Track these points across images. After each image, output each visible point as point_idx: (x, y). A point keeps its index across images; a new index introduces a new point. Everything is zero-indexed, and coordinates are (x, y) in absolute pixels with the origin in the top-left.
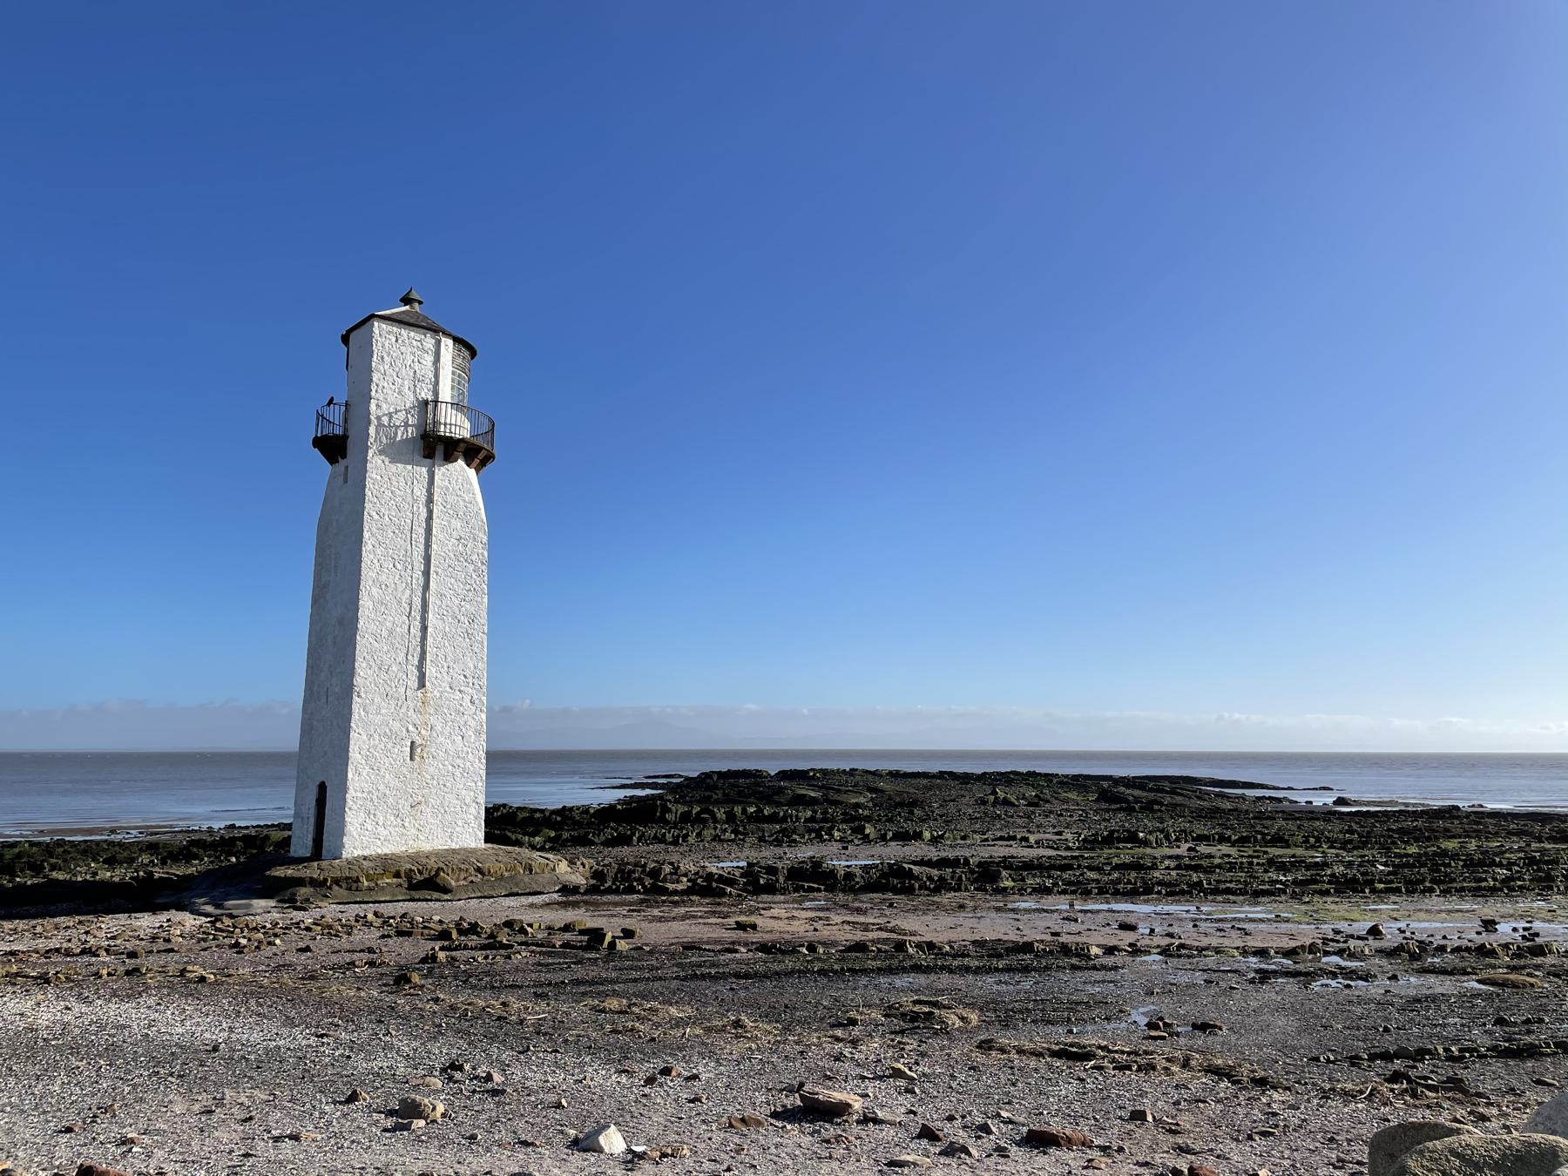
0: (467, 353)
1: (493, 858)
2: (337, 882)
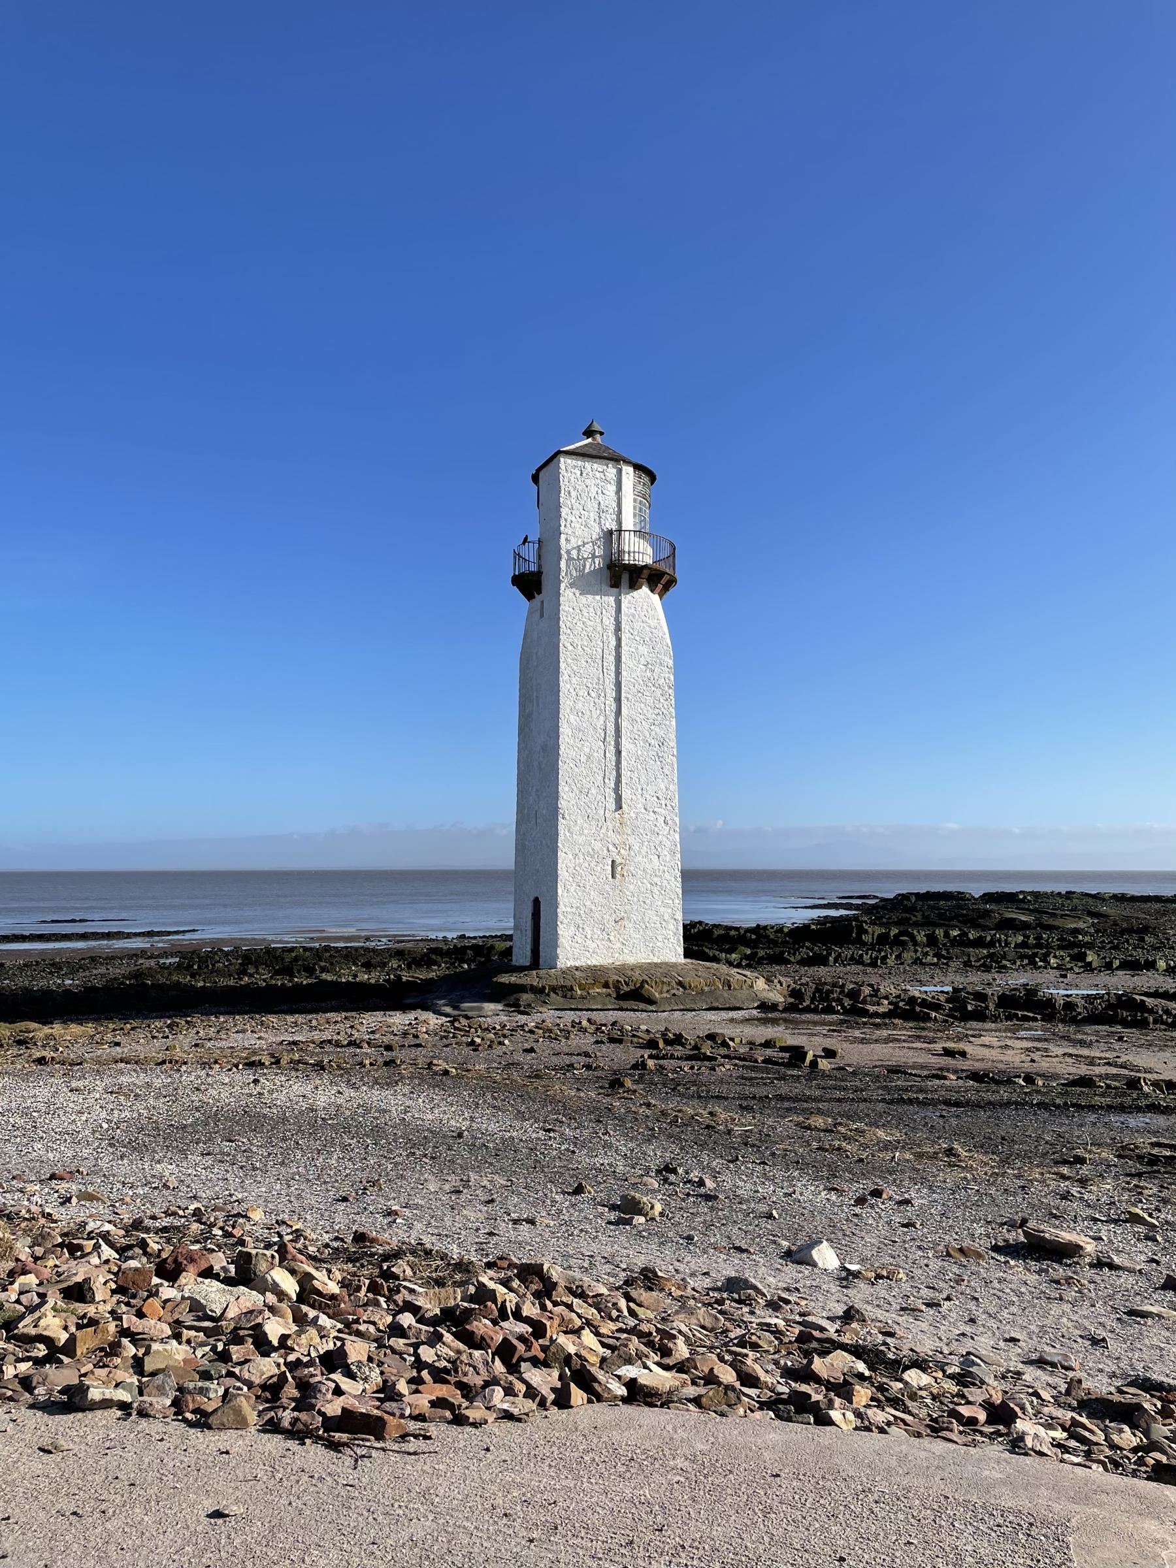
0: (646, 479)
1: (693, 973)
2: (554, 989)
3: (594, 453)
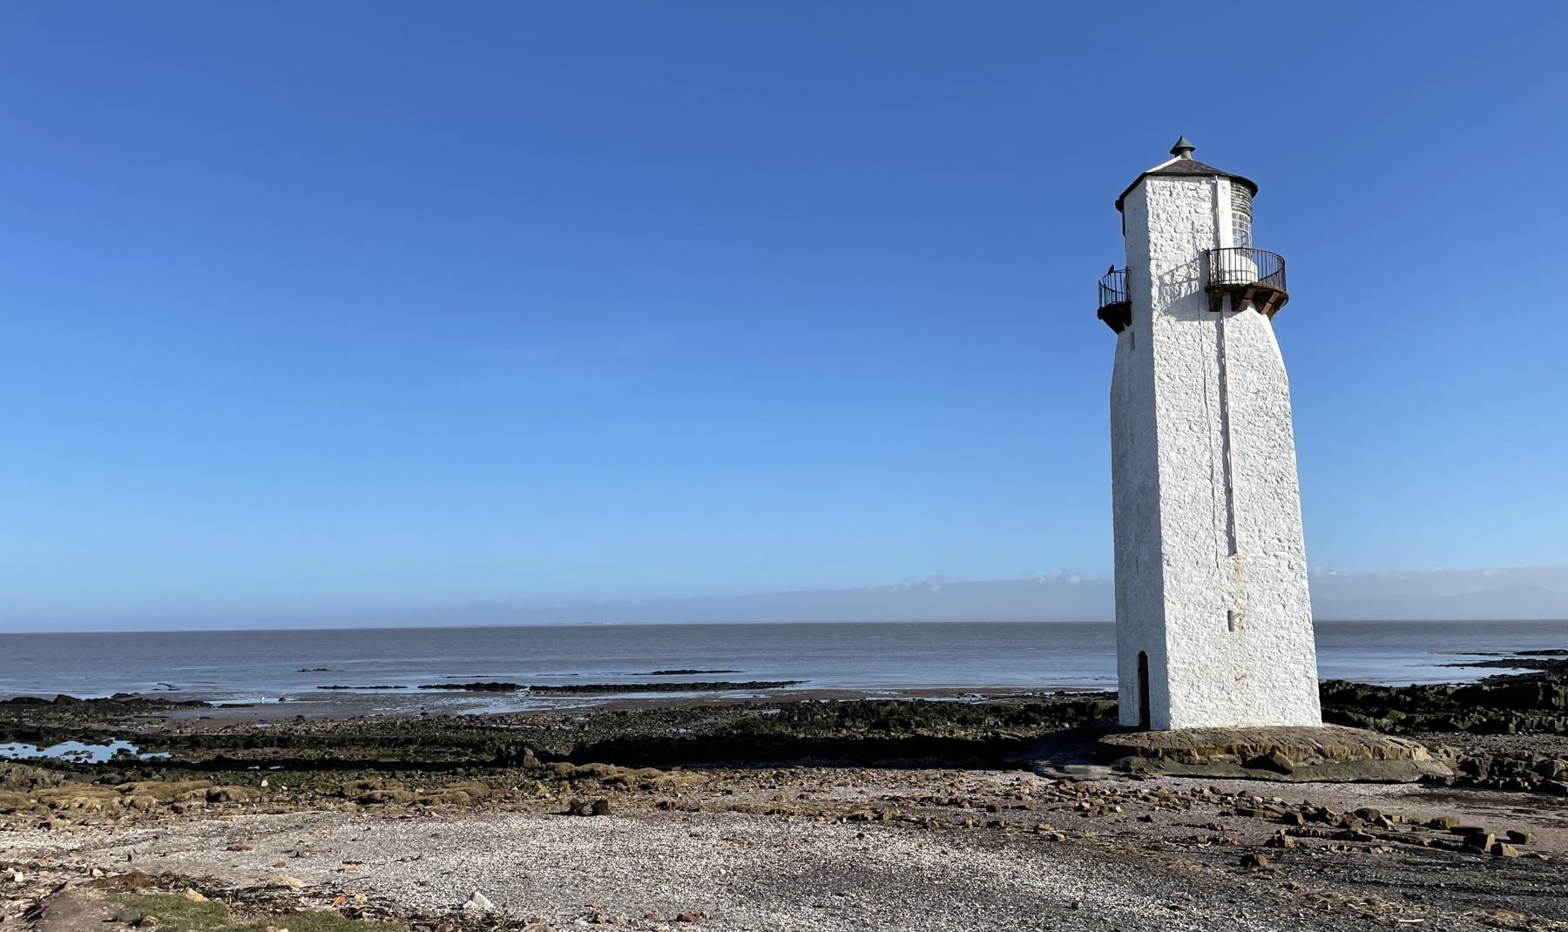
0: (1246, 191)
1: (1335, 739)
2: (1168, 753)
3: (1185, 171)
